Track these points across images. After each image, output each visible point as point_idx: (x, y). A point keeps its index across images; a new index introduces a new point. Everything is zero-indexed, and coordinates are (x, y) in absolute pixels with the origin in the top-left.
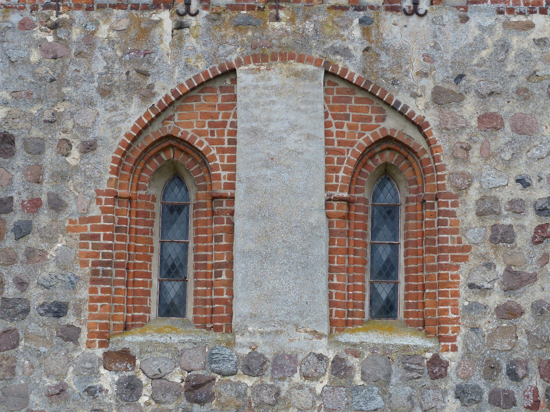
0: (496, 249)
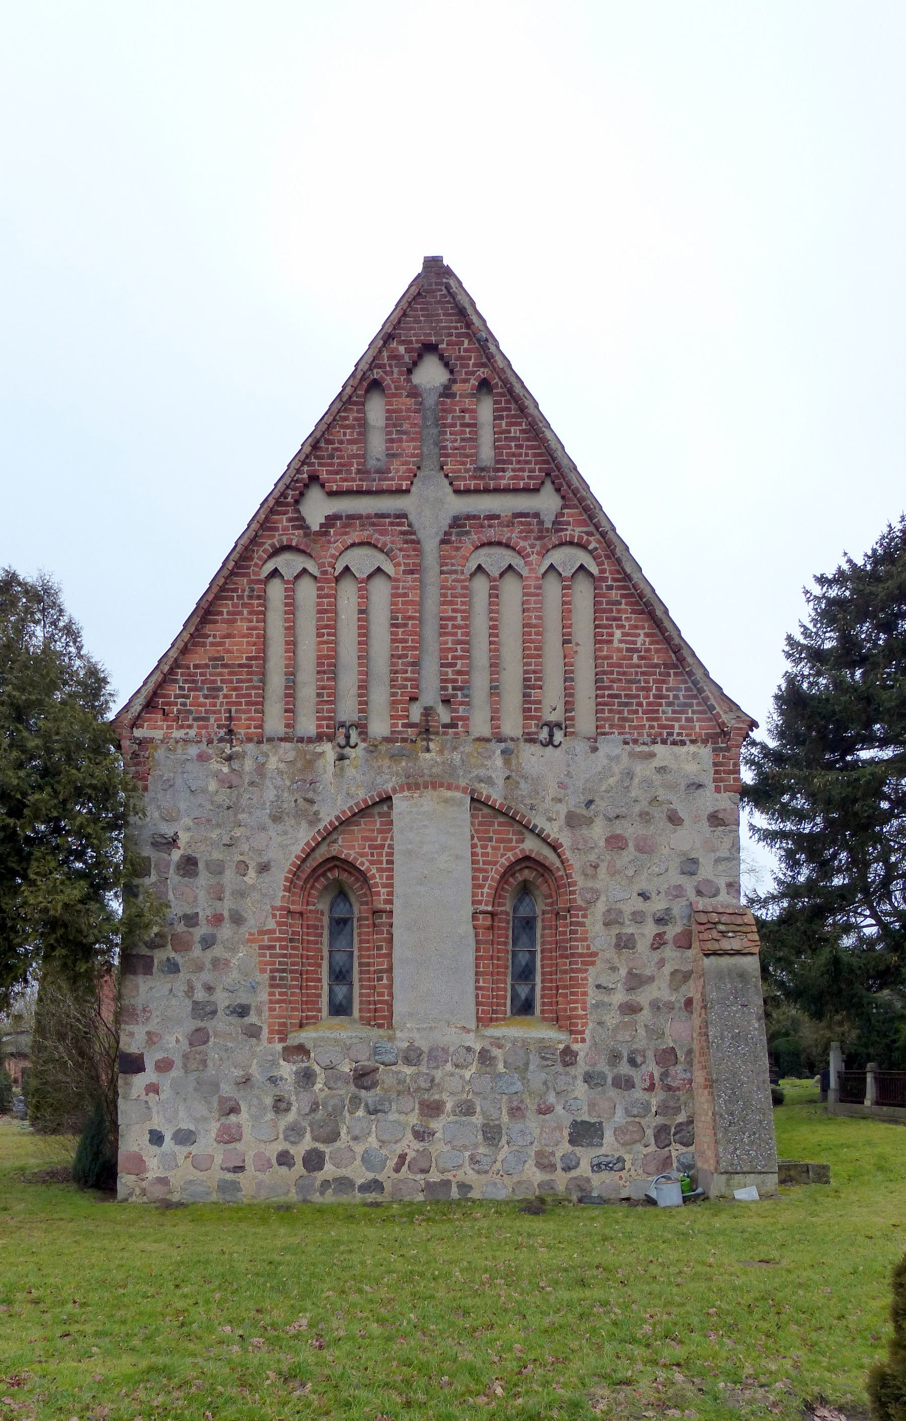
0: (620, 954)
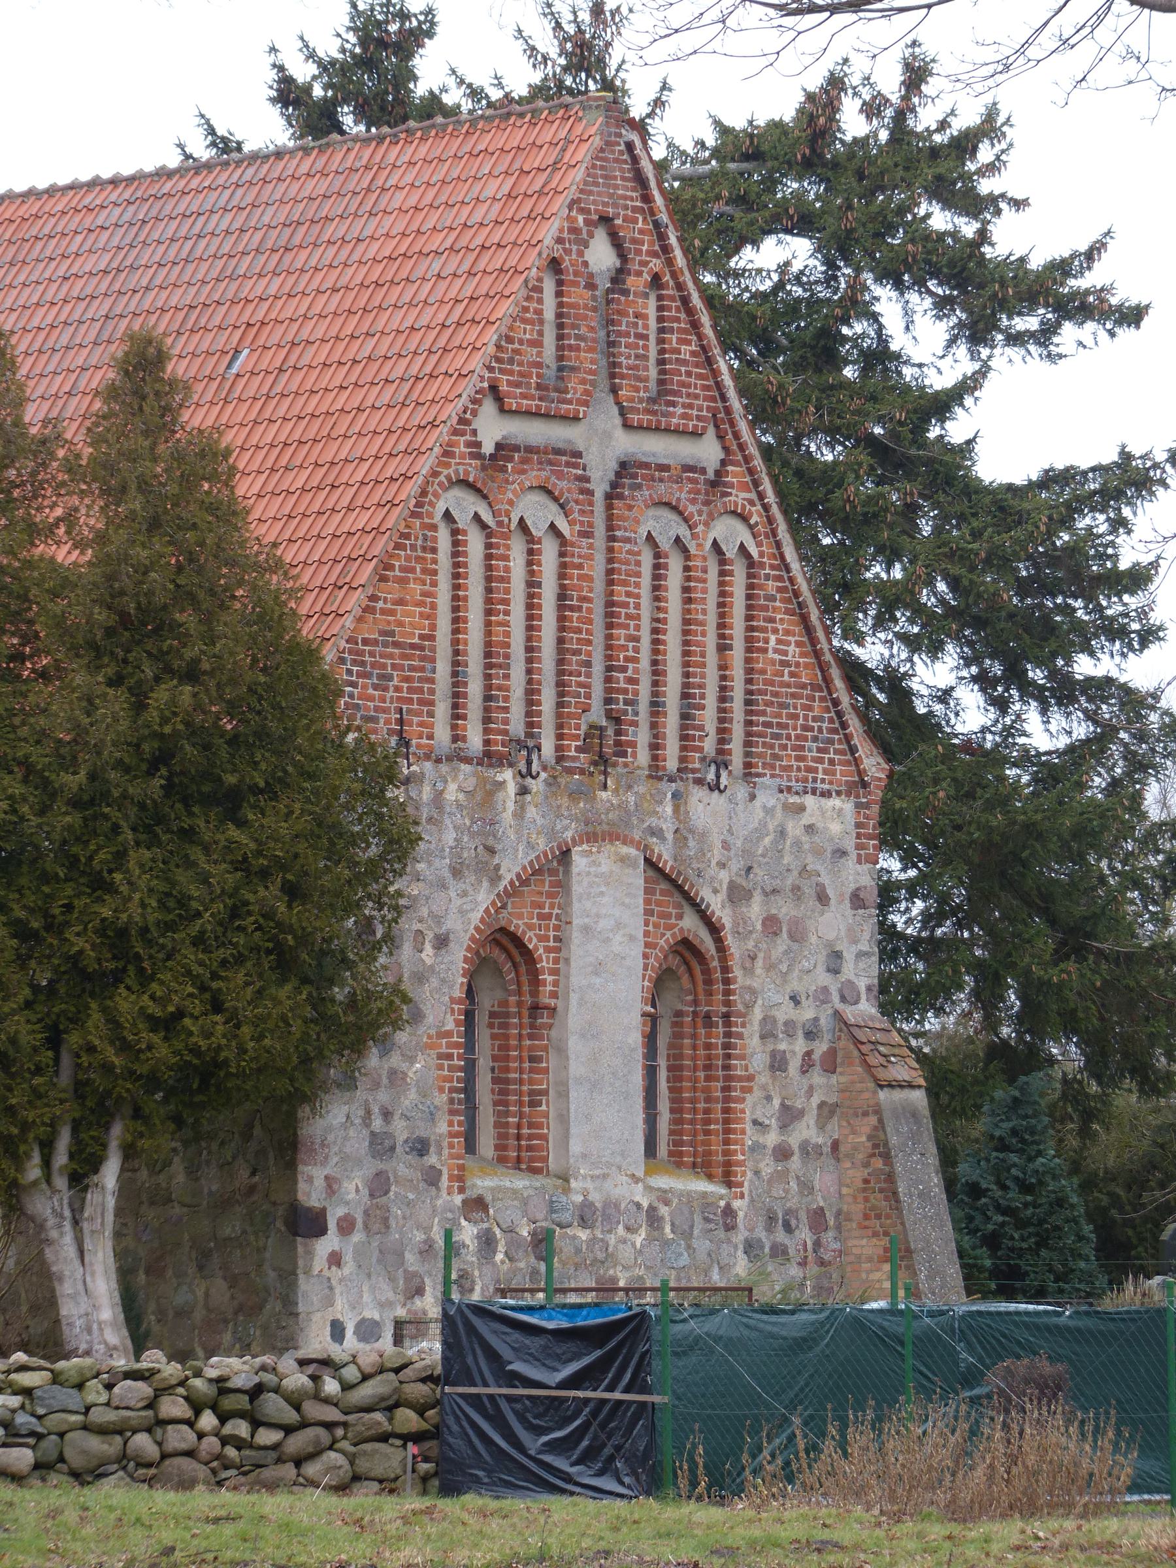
0: (774, 1078)
